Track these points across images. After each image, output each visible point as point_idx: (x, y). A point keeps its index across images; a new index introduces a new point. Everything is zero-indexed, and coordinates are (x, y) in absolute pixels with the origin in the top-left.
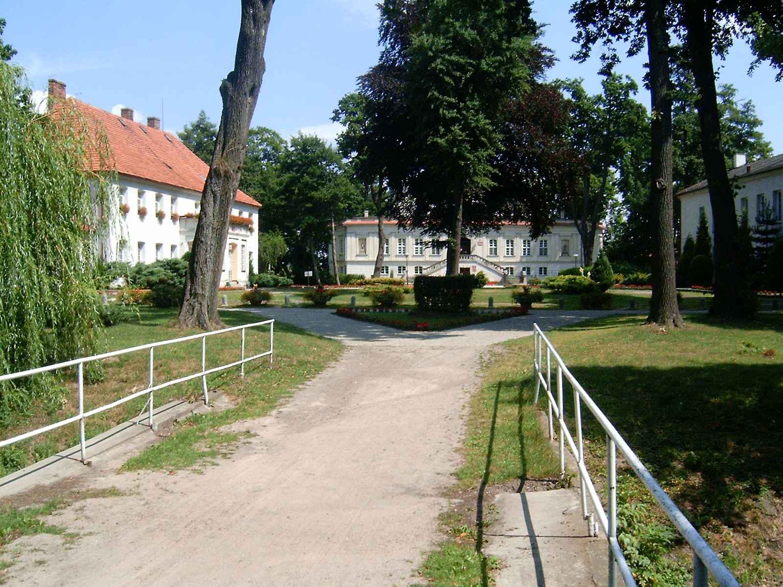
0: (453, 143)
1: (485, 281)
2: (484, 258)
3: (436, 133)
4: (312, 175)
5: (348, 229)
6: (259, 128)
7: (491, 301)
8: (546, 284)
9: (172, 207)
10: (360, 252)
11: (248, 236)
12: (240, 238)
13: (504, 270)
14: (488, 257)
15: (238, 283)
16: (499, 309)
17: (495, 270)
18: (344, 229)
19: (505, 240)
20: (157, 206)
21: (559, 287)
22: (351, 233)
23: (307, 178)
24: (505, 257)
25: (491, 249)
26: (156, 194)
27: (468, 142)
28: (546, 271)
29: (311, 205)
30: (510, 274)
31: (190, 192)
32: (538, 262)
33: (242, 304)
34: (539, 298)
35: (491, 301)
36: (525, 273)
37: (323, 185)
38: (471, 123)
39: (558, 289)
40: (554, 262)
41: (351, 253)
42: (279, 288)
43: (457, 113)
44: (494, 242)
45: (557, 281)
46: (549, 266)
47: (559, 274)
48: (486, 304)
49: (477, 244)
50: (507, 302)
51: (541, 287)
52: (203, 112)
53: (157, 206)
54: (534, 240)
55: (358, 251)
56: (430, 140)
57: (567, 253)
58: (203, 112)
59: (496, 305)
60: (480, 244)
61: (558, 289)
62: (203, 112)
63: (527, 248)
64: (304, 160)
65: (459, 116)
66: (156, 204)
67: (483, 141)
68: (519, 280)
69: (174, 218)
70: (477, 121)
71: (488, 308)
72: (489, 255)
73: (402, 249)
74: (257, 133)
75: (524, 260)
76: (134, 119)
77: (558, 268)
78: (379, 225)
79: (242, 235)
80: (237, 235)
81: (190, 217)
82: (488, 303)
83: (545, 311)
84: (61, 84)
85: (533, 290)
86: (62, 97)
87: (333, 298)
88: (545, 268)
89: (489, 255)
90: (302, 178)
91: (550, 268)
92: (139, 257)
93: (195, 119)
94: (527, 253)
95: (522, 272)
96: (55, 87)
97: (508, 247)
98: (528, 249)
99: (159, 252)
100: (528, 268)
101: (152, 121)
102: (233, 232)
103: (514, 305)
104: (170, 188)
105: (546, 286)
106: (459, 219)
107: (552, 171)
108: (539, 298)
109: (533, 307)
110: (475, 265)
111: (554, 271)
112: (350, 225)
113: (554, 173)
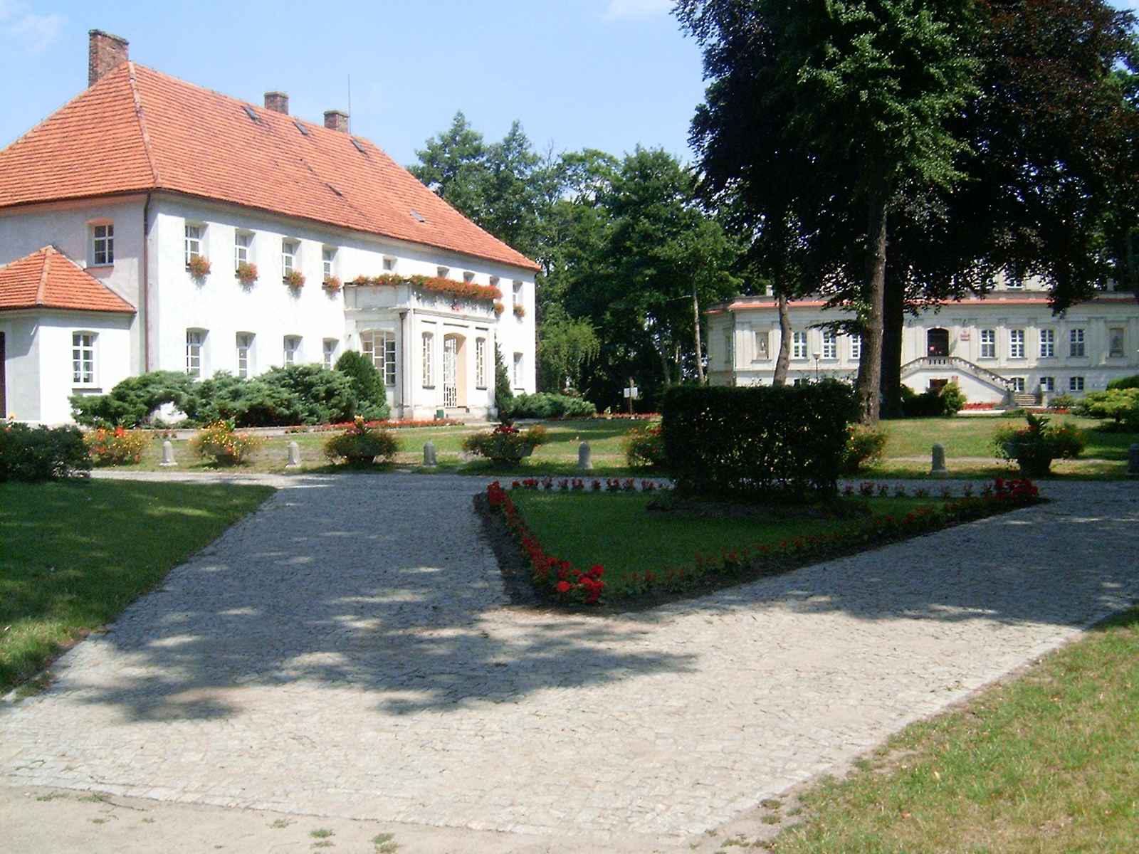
0: (860, 77)
1: (959, 402)
2: (972, 362)
3: (819, 60)
4: (655, 218)
5: (737, 316)
6: (586, 151)
7: (938, 454)
8: (1087, 406)
9: (514, 296)
10: (759, 355)
11: (491, 322)
12: (473, 324)
13: (1008, 382)
14: (979, 360)
15: (468, 410)
16: (958, 476)
17: (992, 382)
18: (730, 317)
19: (1010, 331)
20: (514, 300)
21: (1119, 414)
22: (743, 323)
23: (645, 223)
24: (1008, 359)
25: (984, 346)
26: (284, 239)
27: (893, 74)
28: (1082, 383)
29: (655, 272)
30: (1018, 390)
31: (368, 237)
32: (1066, 368)
33: (327, 463)
34: (1068, 445)
35: (938, 454)
36: (1044, 388)
37: (674, 235)
38: (904, 31)
39: (1118, 420)
40: (1097, 368)
41: (744, 359)
42: (566, 420)
43: (867, 10)
44: (989, 334)
45: (1111, 401)
46: (1087, 375)
47: (1109, 388)
48: (923, 462)
49: (959, 339)
50: (985, 456)
51: (1075, 414)
52: (461, 115)
53: (514, 300)
54: (1059, 315)
55: (755, 354)
56: (804, 75)
57: (1118, 352)
58: (460, 114)
59: (952, 464)
60: (965, 338)
61: (1118, 420)
62: (460, 114)
63: (1047, 343)
64: (641, 193)
65: (871, 15)
66: (514, 296)
67: (932, 76)
68: (1034, 400)
69: (330, 286)
70: (918, 24)
71: (930, 476)
72: (981, 357)
73: (830, 349)
74: (581, 160)
75: (1046, 364)
76: (289, 112)
77: (1105, 378)
78: (781, 307)
79: (478, 320)
80: (464, 318)
81: (362, 285)
82: (930, 460)
83: (1090, 486)
84: (115, 40)
85: (1056, 422)
86: (116, 63)
87: (536, 448)
88: (1081, 379)
89: (981, 357)
90: (637, 225)
91: (1089, 377)
92: (515, 373)
93: (446, 128)
94: (1048, 351)
95: (1039, 386)
96: (100, 44)
97: (1014, 343)
98: (1051, 346)
99: (518, 366)
100: (1051, 380)
101: (331, 118)
102: (454, 312)
103: (1003, 464)
104: (320, 228)
105: (1086, 412)
106: (877, 259)
107: (1097, 158)
108: (1068, 445)
109: (1054, 470)
110: (955, 374)
111: (1096, 383)
112: (741, 311)
113: (1101, 163)
